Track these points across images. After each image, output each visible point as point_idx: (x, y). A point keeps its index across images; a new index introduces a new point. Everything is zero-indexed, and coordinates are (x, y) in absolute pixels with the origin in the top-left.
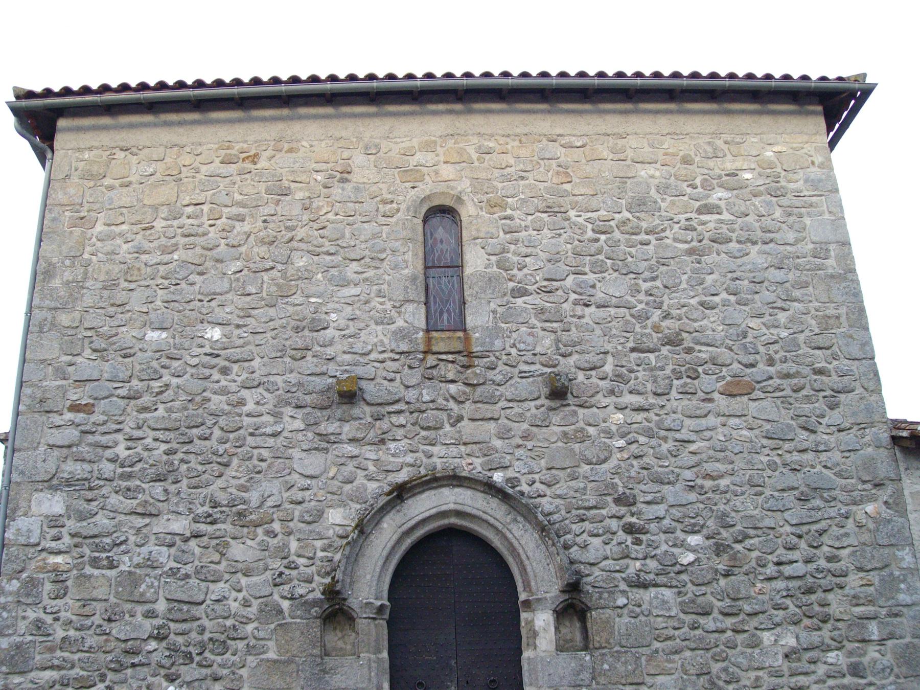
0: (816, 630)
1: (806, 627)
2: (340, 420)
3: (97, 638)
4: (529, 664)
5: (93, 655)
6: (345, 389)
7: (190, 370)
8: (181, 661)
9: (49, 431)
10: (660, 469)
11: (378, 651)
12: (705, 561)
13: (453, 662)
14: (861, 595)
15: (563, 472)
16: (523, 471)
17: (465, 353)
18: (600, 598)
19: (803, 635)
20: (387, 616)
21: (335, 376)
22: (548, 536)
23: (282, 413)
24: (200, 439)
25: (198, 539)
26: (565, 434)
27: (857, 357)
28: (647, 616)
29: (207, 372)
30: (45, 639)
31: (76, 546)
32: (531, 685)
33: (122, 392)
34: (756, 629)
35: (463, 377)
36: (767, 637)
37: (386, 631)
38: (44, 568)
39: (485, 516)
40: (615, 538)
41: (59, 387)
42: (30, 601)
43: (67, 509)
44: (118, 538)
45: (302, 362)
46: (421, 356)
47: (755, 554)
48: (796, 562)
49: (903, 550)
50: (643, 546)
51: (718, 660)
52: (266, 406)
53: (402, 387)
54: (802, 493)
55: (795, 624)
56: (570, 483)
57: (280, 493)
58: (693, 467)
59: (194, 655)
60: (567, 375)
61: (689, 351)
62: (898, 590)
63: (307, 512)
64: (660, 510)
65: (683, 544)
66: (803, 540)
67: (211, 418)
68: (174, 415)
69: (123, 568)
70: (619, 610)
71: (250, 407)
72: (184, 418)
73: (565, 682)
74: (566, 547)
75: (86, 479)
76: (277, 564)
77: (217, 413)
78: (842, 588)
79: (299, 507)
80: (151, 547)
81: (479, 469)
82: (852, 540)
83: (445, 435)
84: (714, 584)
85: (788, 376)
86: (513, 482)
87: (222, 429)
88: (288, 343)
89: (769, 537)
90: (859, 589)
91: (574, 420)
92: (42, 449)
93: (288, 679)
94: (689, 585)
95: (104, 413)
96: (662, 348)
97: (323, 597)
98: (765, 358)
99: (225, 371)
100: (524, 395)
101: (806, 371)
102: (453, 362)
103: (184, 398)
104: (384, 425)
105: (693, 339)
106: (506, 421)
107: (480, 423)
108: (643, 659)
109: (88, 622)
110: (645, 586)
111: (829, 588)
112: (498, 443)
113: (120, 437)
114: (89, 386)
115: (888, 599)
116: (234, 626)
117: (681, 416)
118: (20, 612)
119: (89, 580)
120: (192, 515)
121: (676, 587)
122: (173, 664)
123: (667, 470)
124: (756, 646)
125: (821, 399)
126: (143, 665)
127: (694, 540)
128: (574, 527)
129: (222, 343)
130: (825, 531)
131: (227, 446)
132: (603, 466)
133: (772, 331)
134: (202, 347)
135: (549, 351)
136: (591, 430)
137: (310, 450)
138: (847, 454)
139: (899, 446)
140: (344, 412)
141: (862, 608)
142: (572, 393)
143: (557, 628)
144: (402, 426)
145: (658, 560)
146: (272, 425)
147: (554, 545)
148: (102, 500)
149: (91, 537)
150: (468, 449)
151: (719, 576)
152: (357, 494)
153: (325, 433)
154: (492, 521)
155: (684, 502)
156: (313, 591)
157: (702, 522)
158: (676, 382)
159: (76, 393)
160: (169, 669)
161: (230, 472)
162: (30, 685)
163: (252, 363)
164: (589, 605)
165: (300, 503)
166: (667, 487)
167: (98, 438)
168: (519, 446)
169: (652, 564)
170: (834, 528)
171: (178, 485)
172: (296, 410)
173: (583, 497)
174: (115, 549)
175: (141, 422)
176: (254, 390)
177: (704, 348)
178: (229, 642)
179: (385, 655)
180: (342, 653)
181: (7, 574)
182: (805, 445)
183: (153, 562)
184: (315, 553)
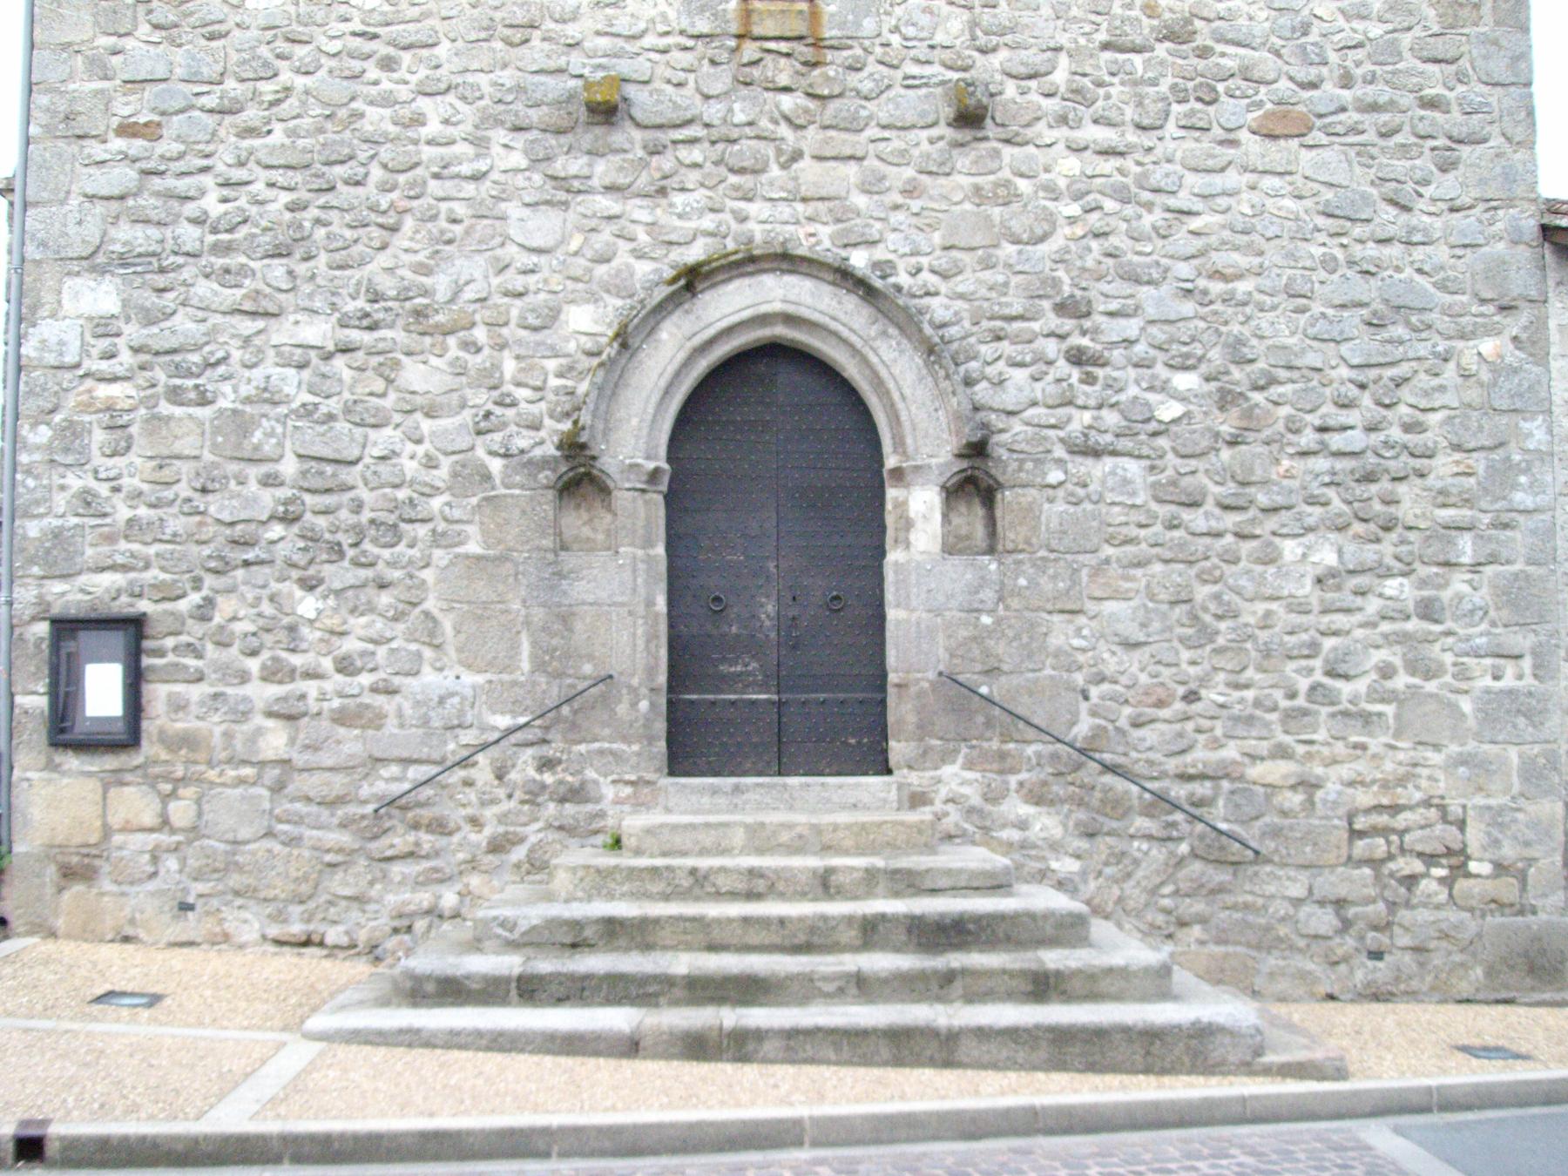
0: (1371, 541)
1: (1357, 536)
2: (589, 153)
3: (183, 519)
4: (896, 572)
5: (178, 547)
6: (599, 98)
7: (328, 63)
8: (325, 557)
9: (85, 170)
10: (1136, 258)
11: (648, 543)
12: (1199, 417)
13: (771, 565)
14: (1454, 490)
15: (971, 254)
16: (902, 251)
17: (810, 41)
18: (1020, 469)
19: (1350, 548)
20: (664, 487)
21: (581, 76)
22: (938, 362)
23: (488, 140)
24: (346, 183)
25: (348, 355)
26: (977, 189)
27: (1502, 79)
28: (1096, 503)
29: (357, 65)
30: (99, 521)
31: (142, 368)
32: (898, 606)
33: (210, 101)
34: (1274, 534)
35: (804, 82)
36: (1290, 549)
37: (662, 512)
38: (90, 405)
39: (833, 325)
40: (1052, 371)
41: (96, 93)
42: (70, 459)
43: (124, 306)
44: (212, 353)
45: (523, 50)
46: (732, 43)
47: (1284, 411)
48: (1351, 428)
49: (1533, 419)
50: (1098, 387)
51: (1206, 582)
52: (461, 127)
53: (698, 98)
54: (1375, 313)
55: (1339, 529)
56: (980, 275)
57: (486, 277)
58: (1193, 257)
59: (345, 547)
60: (987, 85)
61: (1204, 53)
62: (1515, 486)
63: (533, 310)
64: (1131, 327)
65: (1163, 388)
66: (1367, 394)
67: (365, 146)
68: (301, 143)
69: (223, 403)
70: (1050, 492)
71: (433, 128)
72: (318, 147)
73: (953, 604)
74: (969, 382)
75: (154, 254)
76: (481, 398)
77: (376, 138)
78: (1422, 476)
79: (518, 302)
80: (269, 368)
81: (827, 244)
82: (1450, 399)
83: (771, 184)
84: (1212, 456)
85: (1374, 107)
86: (885, 268)
87: (385, 166)
88: (498, 15)
89: (1311, 385)
90: (1450, 480)
91: (995, 165)
92: (74, 202)
93: (501, 587)
94: (1170, 456)
95: (178, 138)
96: (1158, 45)
97: (558, 453)
98: (1337, 73)
99: (388, 64)
100: (910, 118)
101: (1407, 100)
102: (788, 55)
103: (318, 111)
104: (666, 163)
105: (1213, 32)
106: (877, 163)
107: (832, 164)
108: (1085, 572)
109: (169, 494)
110: (1096, 453)
111: (1402, 474)
112: (860, 201)
113: (208, 180)
114: (151, 90)
115: (1496, 500)
116: (411, 500)
117: (1178, 168)
118: (55, 477)
119: (167, 423)
120: (337, 315)
121: (1148, 457)
122: (311, 562)
123: (1148, 259)
124: (1272, 561)
125: (1427, 152)
126: (261, 563)
127: (1185, 381)
128: (983, 349)
129: (382, 13)
130: (1407, 380)
131: (394, 195)
132: (1040, 247)
133: (1356, 24)
134: (347, 20)
135: (958, 42)
136: (1023, 185)
137: (537, 203)
138: (1459, 252)
139: (1552, 243)
140: (596, 139)
141: (1451, 512)
142: (993, 118)
143: (945, 516)
144: (696, 166)
145: (1122, 412)
146: (471, 161)
147: (947, 377)
148: (182, 289)
149: (167, 352)
150: (808, 209)
151: (1220, 444)
152: (618, 281)
153: (562, 174)
154: (845, 333)
155: (1173, 317)
156: (542, 443)
157: (1199, 352)
158: (1176, 108)
159: (127, 104)
160: (304, 569)
161: (400, 241)
162: (80, 596)
163: (436, 51)
164: (1001, 479)
165: (520, 295)
166: (1145, 289)
167: (170, 182)
168: (896, 207)
169: (1111, 418)
170: (1422, 376)
171: (311, 264)
172: (512, 135)
173: (1003, 299)
174: (208, 373)
175: (244, 154)
176: (439, 98)
177: (1231, 50)
178: (403, 526)
179: (660, 550)
180: (590, 546)
181: (28, 417)
182: (1391, 231)
183: (273, 394)
184: (545, 381)
